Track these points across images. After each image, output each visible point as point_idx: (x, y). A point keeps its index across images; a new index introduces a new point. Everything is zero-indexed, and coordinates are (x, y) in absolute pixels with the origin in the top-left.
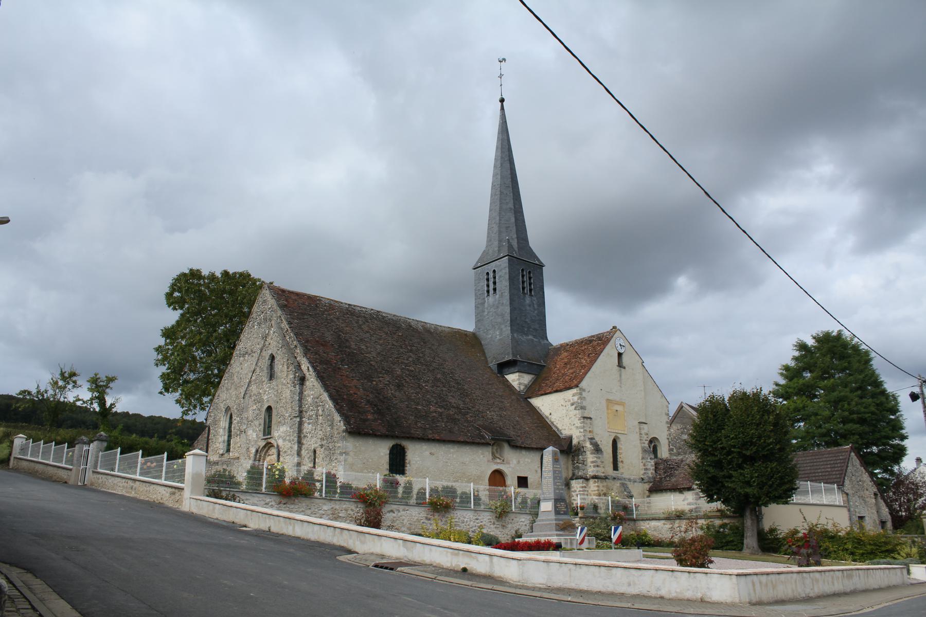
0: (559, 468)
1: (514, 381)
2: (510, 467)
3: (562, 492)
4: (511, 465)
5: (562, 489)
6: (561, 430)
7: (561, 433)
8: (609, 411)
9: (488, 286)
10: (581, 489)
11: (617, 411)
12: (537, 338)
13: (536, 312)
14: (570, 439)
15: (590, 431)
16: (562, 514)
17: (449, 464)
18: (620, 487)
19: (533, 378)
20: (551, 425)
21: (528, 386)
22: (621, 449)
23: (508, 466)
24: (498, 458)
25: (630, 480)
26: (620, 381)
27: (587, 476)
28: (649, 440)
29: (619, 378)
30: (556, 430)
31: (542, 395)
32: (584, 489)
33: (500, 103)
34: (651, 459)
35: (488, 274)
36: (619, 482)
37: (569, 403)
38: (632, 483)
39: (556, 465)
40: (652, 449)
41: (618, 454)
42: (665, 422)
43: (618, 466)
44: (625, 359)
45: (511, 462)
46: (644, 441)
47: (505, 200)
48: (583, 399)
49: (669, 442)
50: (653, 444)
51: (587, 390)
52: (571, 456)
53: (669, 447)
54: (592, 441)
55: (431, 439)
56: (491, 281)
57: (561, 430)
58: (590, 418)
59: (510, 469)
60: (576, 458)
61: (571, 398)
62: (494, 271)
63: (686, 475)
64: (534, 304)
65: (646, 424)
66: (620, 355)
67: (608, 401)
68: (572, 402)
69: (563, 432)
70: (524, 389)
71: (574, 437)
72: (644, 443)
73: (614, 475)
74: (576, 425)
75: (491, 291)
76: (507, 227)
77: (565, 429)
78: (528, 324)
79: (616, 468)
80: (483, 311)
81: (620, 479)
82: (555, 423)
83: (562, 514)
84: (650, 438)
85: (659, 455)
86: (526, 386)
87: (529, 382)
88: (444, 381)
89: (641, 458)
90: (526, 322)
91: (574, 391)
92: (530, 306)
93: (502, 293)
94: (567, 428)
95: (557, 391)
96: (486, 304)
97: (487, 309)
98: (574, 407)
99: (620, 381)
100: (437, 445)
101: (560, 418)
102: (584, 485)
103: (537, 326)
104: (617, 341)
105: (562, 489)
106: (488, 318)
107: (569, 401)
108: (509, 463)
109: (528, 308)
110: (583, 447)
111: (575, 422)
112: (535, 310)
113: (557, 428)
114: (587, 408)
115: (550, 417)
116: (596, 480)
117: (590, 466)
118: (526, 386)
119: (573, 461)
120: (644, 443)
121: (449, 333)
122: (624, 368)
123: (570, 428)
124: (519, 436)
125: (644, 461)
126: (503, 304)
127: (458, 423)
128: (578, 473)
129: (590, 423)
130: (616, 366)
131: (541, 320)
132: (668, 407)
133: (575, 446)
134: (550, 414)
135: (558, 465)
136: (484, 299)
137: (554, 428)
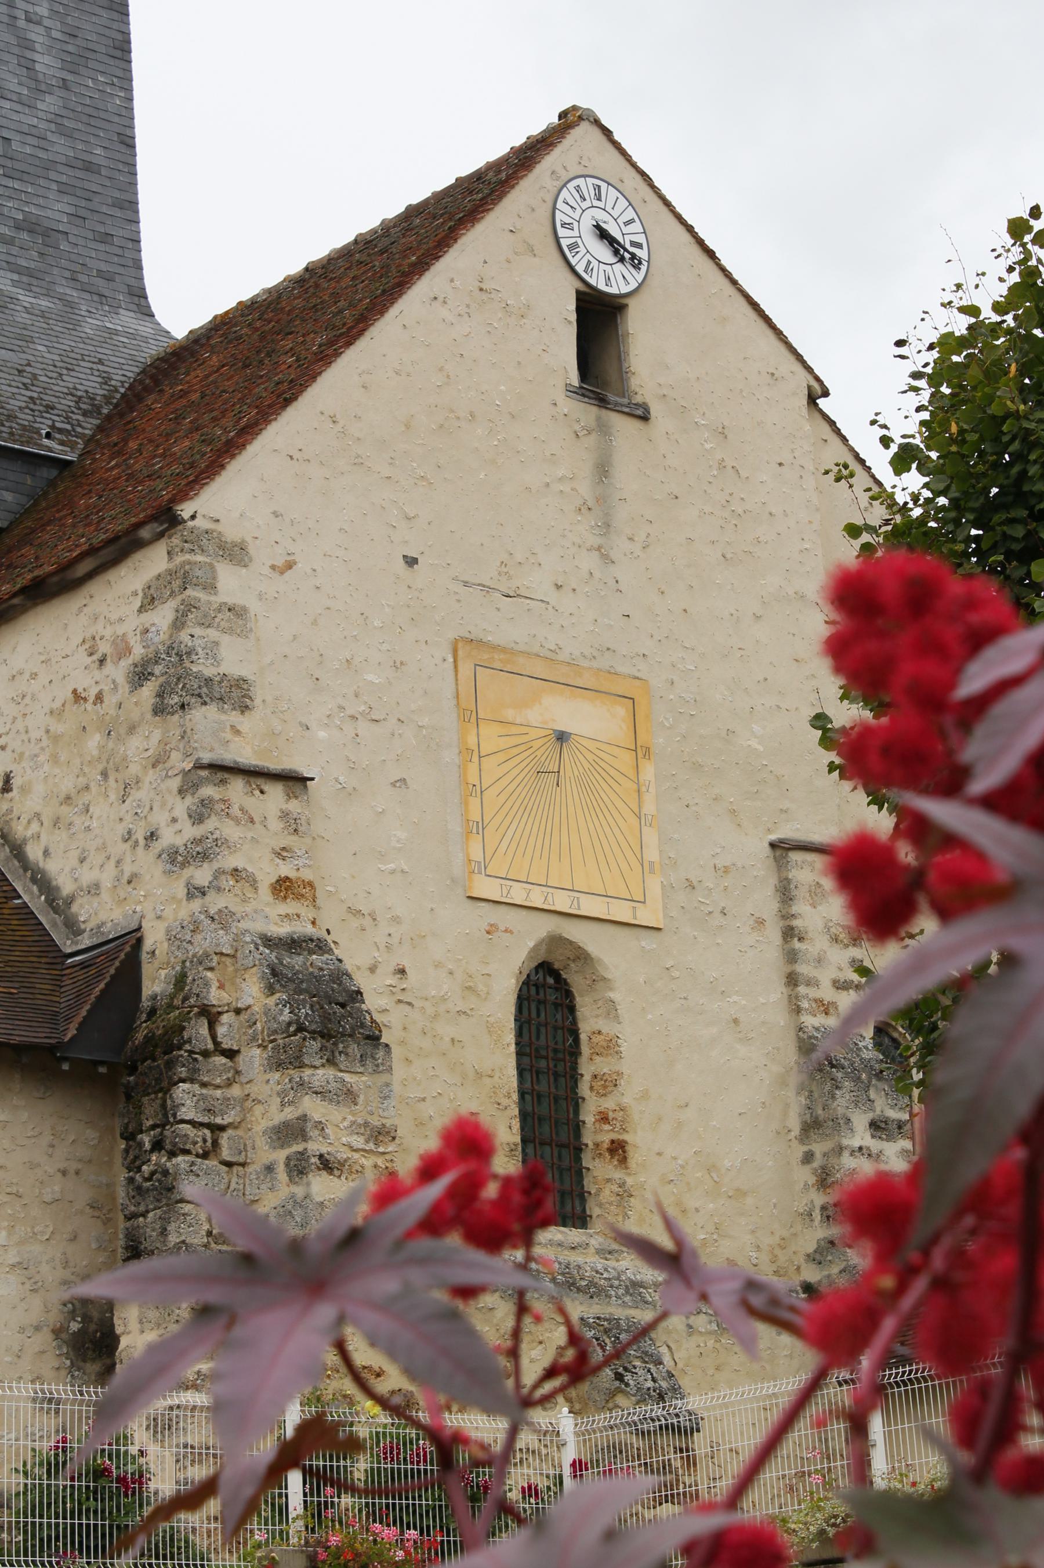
6: (70, 901)
7: (73, 927)
8: (490, 737)
11: (562, 737)
13: (49, 103)
15: (284, 887)
22: (610, 1047)
29: (585, 489)
34: (877, 1126)
37: (118, 672)
41: (584, 1089)
43: (589, 1185)
46: (827, 993)
51: (263, 556)
54: (297, 961)
61: (131, 625)
64: (27, 44)
68: (138, 651)
69: (84, 910)
71: (154, 937)
74: (168, 838)
77: (94, 889)
82: (34, 852)
89: (795, 1124)
98: (148, 692)
111: (159, 818)
112: (39, 88)
113: (43, 883)
114: (260, 694)
117: (270, 1169)
123: (128, 869)
125: (819, 1148)
128: (164, 1232)
129: (285, 815)
130: (560, 395)
131: (89, 167)
133: (152, 1012)
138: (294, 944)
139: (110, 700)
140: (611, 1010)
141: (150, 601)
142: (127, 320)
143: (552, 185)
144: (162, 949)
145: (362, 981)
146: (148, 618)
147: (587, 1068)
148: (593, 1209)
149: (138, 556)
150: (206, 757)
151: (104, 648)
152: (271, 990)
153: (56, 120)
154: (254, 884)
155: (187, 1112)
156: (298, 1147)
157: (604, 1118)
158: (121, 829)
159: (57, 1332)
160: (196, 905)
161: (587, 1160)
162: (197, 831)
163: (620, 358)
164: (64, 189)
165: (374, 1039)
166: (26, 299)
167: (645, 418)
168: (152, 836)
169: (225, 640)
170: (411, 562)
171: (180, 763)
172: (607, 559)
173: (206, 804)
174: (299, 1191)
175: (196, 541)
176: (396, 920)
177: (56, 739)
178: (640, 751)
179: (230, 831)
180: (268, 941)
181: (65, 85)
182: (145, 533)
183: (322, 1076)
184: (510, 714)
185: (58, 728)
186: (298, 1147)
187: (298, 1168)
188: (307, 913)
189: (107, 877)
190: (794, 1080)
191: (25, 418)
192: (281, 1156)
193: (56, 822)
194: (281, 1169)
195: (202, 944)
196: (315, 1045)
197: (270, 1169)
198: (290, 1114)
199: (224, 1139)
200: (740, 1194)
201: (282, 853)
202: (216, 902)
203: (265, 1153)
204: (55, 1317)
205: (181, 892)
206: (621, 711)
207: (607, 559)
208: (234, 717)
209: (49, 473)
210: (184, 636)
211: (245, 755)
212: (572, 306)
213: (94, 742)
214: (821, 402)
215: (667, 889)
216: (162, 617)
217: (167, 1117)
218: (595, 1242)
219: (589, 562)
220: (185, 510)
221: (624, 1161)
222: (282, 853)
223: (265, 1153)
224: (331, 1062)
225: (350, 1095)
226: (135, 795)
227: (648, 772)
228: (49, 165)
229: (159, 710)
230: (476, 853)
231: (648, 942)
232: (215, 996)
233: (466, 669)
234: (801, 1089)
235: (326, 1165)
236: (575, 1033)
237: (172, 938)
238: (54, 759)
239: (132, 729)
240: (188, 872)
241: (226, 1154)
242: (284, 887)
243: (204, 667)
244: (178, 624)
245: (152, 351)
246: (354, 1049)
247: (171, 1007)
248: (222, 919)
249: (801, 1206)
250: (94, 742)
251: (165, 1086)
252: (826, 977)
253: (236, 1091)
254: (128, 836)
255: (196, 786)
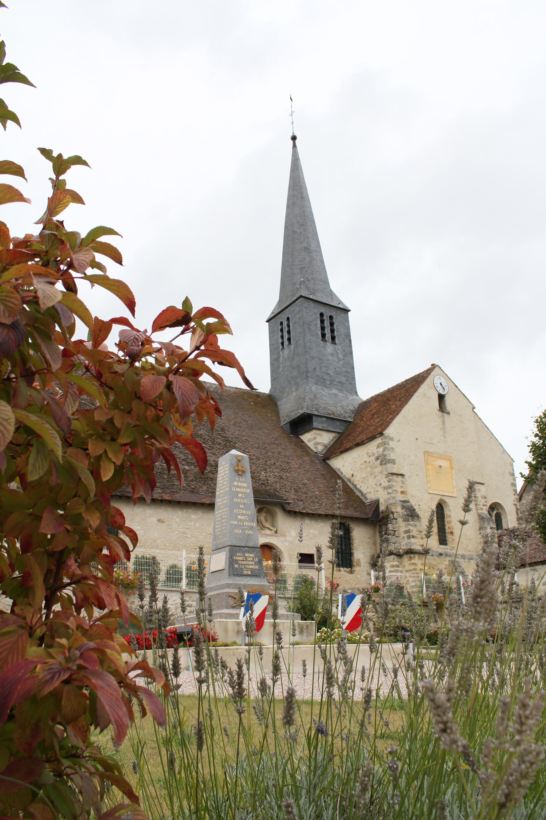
0: (245, 487)
1: (309, 441)
2: (286, 541)
3: (251, 532)
4: (288, 538)
5: (251, 528)
6: (365, 494)
7: (366, 498)
8: (430, 467)
9: (282, 337)
10: (392, 569)
11: (440, 466)
12: (343, 393)
13: (341, 362)
14: (376, 503)
15: (402, 492)
16: (248, 575)
17: (189, 536)
18: (449, 565)
19: (335, 437)
20: (354, 490)
21: (329, 447)
22: (450, 516)
23: (283, 539)
24: (268, 528)
25: (463, 557)
26: (444, 429)
27: (399, 552)
28: (488, 505)
29: (441, 426)
30: (359, 495)
31: (342, 452)
32: (395, 569)
33: (292, 142)
35: (281, 323)
36: (448, 559)
37: (373, 458)
38: (466, 560)
39: (239, 481)
40: (494, 518)
41: (446, 523)
42: (509, 483)
43: (447, 538)
44: (449, 402)
45: (288, 534)
46: (482, 507)
47: (299, 239)
48: (391, 450)
49: (517, 509)
50: (495, 512)
51: (396, 439)
52: (378, 526)
53: (518, 514)
54: (405, 504)
55: (157, 499)
56: (286, 330)
57: (365, 494)
58: (402, 475)
59: (287, 544)
60: (384, 528)
62: (288, 319)
63: (539, 546)
64: (337, 353)
65: (483, 484)
66: (441, 397)
67: (426, 453)
68: (376, 455)
69: (368, 496)
70: (323, 450)
71: (381, 501)
72: (482, 509)
73: (440, 551)
74: (383, 485)
75: (286, 343)
76: (301, 268)
77: (370, 493)
78: (331, 376)
79: (443, 541)
80: (279, 367)
81: (450, 556)
82: (358, 487)
83: (248, 575)
84: (490, 503)
85: (504, 526)
86: (325, 446)
87: (330, 442)
88: (207, 437)
89: (478, 529)
90: (328, 374)
91: (379, 441)
92: (332, 355)
93: (297, 342)
94: (372, 491)
95: (358, 445)
96: (281, 358)
97: (282, 364)
98: (379, 461)
99: (444, 429)
100: (170, 509)
101: (364, 478)
102: (396, 563)
103: (343, 379)
104: (435, 379)
105: (251, 528)
106: (283, 374)
107: (373, 454)
108: (284, 536)
109: (330, 358)
110: (393, 513)
111: (382, 482)
112: (340, 360)
113: (360, 492)
114: (397, 462)
115: (352, 479)
116: (412, 556)
117: (404, 537)
118: (325, 446)
119: (380, 532)
120: (482, 509)
121: (235, 393)
122: (449, 413)
123: (376, 490)
124: (302, 500)
125: (482, 532)
126: (298, 354)
127: (210, 482)
129: (402, 481)
131: (348, 372)
132: (512, 466)
133: (383, 513)
134: (353, 476)
135: (242, 482)
136: (279, 353)
137: (358, 493)
138: (404, 502)
139: (372, 463)
140: (450, 510)
141: (378, 447)
142: (355, 397)
143: (433, 377)
144: (383, 502)
145: (415, 507)
146: (378, 449)
147: (446, 520)
148: (448, 542)
149: (376, 440)
150: (390, 472)
151: (370, 454)
152: (403, 509)
153: (342, 365)
154: (398, 492)
155: (390, 529)
156: (409, 534)
157: (449, 528)
158: (375, 483)
159: (369, 563)
160: (389, 496)
161: (447, 535)
162: (389, 484)
163: (444, 404)
164: (344, 376)
165: (418, 516)
166: (340, 394)
167: (449, 414)
168: (380, 484)
169: (391, 453)
170: (417, 439)
171: (385, 473)
172: (445, 437)
173: (390, 479)
174: (409, 541)
175: (386, 437)
176: (418, 497)
177: (362, 469)
178: (452, 468)
179: (394, 484)
180: (401, 501)
181: (343, 359)
182: (377, 436)
183: (412, 523)
184: (433, 463)
185: (362, 467)
186: (409, 534)
187: (409, 537)
188: (406, 497)
189: (372, 491)
190: (477, 521)
191: (344, 414)
192: (405, 535)
193: (362, 482)
194: (406, 537)
195: (390, 502)
196: (410, 518)
197: (404, 537)
198: (407, 529)
199: (396, 533)
200: (470, 540)
201: (401, 487)
202: (393, 495)
203: (403, 535)
204: (369, 561)
205: (386, 493)
206: (449, 462)
207: (445, 437)
208: (393, 465)
209: (348, 423)
210: (385, 453)
211: (395, 471)
212: (437, 396)
213: (369, 469)
214: (474, 410)
215: (457, 490)
216: (381, 450)
217: (387, 529)
218: (449, 548)
219: (442, 438)
220: (384, 433)
221: (453, 535)
222: (401, 487)
223: (403, 535)
224: (413, 521)
225: (416, 526)
226: (377, 478)
227: (453, 471)
228: (342, 372)
229: (381, 464)
230: (429, 486)
231: (454, 499)
232: (393, 510)
233: (426, 456)
234: (478, 522)
235: (413, 537)
236: (444, 514)
237: (385, 500)
238: (361, 472)
239: (376, 467)
240: (387, 490)
241: (396, 535)
242: (402, 492)
243: (388, 458)
244: (384, 451)
245: (360, 402)
246: (416, 518)
247: (386, 512)
248: (394, 498)
249: (479, 541)
250: (369, 469)
251: (386, 524)
252: (481, 504)
253: (397, 525)
254: (376, 484)
255: (388, 477)
